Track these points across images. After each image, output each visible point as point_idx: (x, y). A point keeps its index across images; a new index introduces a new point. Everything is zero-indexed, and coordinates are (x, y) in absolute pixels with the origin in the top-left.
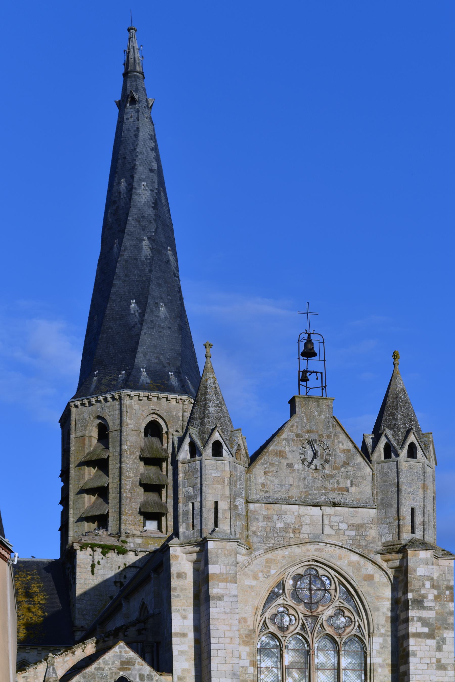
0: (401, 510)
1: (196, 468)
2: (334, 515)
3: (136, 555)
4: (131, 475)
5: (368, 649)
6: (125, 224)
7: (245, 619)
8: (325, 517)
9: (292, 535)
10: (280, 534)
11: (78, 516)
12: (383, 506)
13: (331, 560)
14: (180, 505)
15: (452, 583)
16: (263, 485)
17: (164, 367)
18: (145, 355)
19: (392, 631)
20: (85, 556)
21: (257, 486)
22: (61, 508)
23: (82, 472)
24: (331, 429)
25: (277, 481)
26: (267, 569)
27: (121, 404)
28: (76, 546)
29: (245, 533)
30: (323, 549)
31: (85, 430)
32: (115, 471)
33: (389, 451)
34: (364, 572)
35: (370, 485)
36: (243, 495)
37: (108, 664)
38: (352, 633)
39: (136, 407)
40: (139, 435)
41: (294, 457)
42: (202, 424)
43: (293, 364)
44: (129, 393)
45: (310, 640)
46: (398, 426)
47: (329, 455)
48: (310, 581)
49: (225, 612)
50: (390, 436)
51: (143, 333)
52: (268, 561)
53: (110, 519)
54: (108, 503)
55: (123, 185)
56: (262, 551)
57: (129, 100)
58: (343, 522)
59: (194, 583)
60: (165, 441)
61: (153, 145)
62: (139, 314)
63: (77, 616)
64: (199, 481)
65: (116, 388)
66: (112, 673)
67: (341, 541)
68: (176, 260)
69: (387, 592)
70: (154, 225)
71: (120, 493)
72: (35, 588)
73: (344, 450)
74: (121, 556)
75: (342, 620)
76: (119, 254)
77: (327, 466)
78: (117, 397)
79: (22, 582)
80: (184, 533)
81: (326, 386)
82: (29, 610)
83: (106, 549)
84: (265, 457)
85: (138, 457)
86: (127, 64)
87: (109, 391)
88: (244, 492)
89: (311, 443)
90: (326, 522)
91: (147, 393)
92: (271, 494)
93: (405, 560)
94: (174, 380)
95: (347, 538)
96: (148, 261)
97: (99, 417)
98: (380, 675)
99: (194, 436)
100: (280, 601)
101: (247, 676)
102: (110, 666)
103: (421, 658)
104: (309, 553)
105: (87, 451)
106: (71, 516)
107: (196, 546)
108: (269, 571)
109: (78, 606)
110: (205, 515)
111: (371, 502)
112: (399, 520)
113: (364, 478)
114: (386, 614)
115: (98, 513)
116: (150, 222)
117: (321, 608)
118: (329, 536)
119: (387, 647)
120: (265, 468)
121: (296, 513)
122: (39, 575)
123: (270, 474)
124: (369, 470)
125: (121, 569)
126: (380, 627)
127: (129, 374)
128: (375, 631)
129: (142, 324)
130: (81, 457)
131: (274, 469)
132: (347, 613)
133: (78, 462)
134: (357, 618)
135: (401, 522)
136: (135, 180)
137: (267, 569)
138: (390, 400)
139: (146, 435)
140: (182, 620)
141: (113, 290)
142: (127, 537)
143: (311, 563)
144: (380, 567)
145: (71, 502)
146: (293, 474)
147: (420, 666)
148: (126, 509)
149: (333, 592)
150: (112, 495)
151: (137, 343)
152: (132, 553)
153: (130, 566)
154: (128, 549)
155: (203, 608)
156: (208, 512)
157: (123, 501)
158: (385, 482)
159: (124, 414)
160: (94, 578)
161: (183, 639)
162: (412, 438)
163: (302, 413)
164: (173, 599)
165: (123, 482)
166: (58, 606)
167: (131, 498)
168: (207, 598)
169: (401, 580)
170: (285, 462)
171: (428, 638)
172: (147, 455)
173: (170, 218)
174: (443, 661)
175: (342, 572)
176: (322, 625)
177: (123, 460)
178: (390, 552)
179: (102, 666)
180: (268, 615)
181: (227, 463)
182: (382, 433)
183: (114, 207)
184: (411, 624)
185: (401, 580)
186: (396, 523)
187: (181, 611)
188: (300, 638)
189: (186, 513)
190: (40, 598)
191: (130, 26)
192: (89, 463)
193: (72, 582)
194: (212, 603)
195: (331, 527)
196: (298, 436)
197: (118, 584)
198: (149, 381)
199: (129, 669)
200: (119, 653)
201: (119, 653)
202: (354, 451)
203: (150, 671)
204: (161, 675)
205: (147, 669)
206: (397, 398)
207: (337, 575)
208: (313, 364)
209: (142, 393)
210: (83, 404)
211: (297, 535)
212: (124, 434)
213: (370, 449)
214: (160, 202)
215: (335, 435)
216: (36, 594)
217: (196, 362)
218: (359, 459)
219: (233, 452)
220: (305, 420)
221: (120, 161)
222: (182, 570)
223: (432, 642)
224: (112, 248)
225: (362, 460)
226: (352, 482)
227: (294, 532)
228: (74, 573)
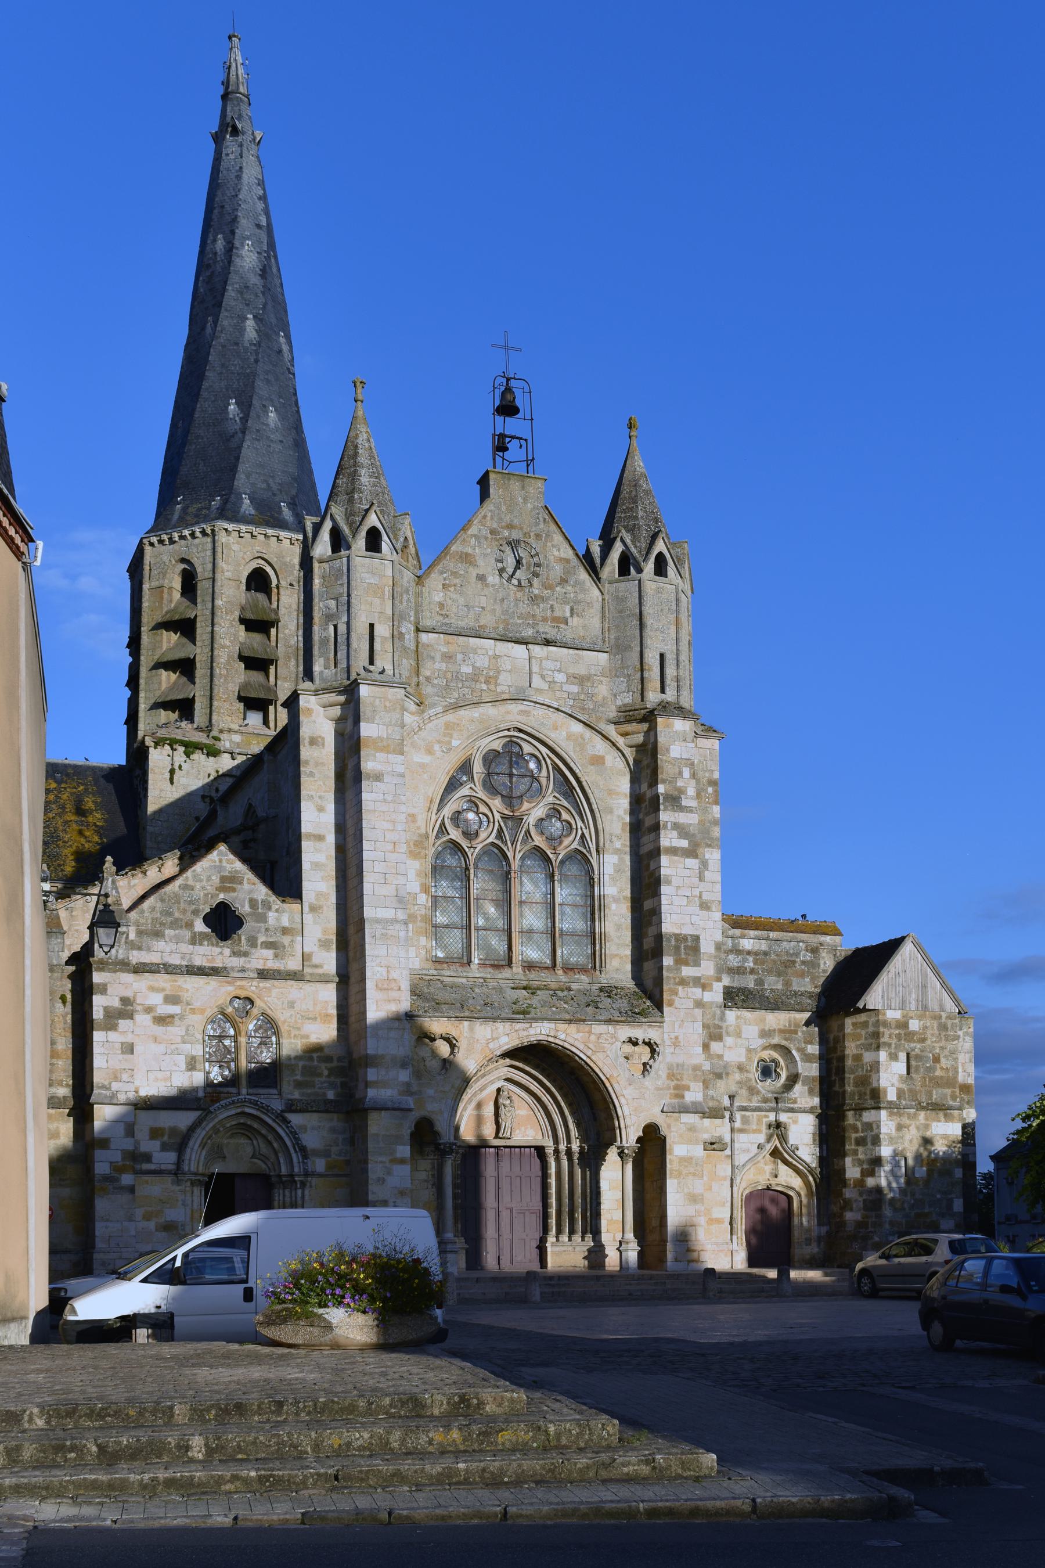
0: (646, 655)
1: (340, 570)
2: (547, 658)
3: (233, 759)
4: (228, 643)
5: (596, 872)
6: (223, 295)
7: (412, 817)
8: (533, 661)
9: (484, 687)
10: (467, 684)
11: (152, 701)
12: (618, 649)
13: (542, 730)
14: (316, 629)
15: (716, 775)
16: (441, 605)
17: (274, 495)
18: (248, 476)
19: (631, 847)
20: (161, 757)
21: (432, 606)
22: (128, 693)
23: (158, 638)
24: (542, 526)
25: (461, 601)
26: (447, 739)
27: (214, 542)
28: (149, 742)
29: (415, 680)
30: (529, 712)
31: (163, 579)
32: (204, 637)
33: (626, 564)
34: (590, 751)
35: (599, 615)
36: (412, 619)
37: (201, 881)
38: (572, 847)
39: (235, 547)
40: (239, 587)
41: (486, 565)
42: (351, 500)
43: (487, 424)
44: (226, 525)
45: (510, 855)
46: (639, 528)
47: (538, 565)
48: (511, 761)
49: (385, 801)
50: (628, 541)
51: (245, 445)
52: (448, 726)
53: (198, 706)
54: (194, 683)
55: (220, 244)
56: (439, 709)
57: (230, 129)
58: (560, 671)
59: (336, 754)
60: (274, 598)
61: (261, 192)
62: (241, 419)
63: (149, 844)
64: (346, 590)
65: (207, 519)
66: (206, 895)
67: (557, 700)
68: (291, 351)
69: (624, 785)
70: (262, 299)
71: (212, 668)
72: (89, 803)
73: (561, 559)
74: (211, 758)
75: (556, 827)
76: (213, 336)
77: (536, 582)
78: (209, 531)
79: (72, 794)
80: (321, 673)
81: (533, 459)
82: (81, 833)
83: (190, 748)
84: (445, 562)
85: (237, 619)
86: (226, 84)
87: (197, 523)
88: (412, 613)
89: (513, 544)
90: (535, 669)
91: (251, 528)
92: (453, 621)
93: (652, 733)
94: (287, 514)
95: (565, 695)
96: (254, 348)
97: (183, 560)
99: (338, 518)
100: (465, 791)
101: (416, 908)
102: (204, 883)
103: (678, 888)
104: (510, 717)
105: (165, 609)
106: (141, 700)
107: (340, 693)
108: (450, 743)
109: (150, 829)
110: (354, 644)
111: (600, 642)
112: (642, 670)
113: (589, 604)
114: (623, 819)
115: (180, 697)
116: (256, 296)
117: (526, 806)
118: (539, 691)
119: (624, 871)
120: (445, 579)
121: (491, 653)
122: (95, 785)
123: (452, 589)
124: (597, 592)
125: (212, 778)
126: (614, 839)
127: (225, 502)
128: (607, 845)
129: (244, 433)
130: (159, 618)
131: (457, 581)
132: (565, 816)
133: (154, 624)
134: (580, 824)
135: (646, 674)
136: (237, 236)
137: (447, 739)
138: (625, 489)
139: (248, 589)
140: (316, 813)
141: (206, 384)
142: (221, 731)
143: (512, 733)
144: (614, 744)
145: (142, 681)
146: (486, 592)
147: (676, 900)
148: (219, 691)
149: (544, 781)
150: (201, 672)
151: (237, 458)
152: (227, 756)
153: (224, 775)
154: (222, 749)
155: (349, 795)
156: (359, 639)
157: (215, 680)
158: (620, 612)
159: (219, 555)
160: (174, 789)
161: (318, 844)
162: (660, 546)
163: (499, 497)
164: (304, 779)
165: (216, 653)
166: (122, 829)
167: (226, 677)
168: (358, 777)
169: (646, 765)
170: (474, 572)
171: (688, 857)
172: (249, 616)
173: (283, 294)
174: (705, 897)
175: (558, 750)
176: (528, 832)
177: (216, 620)
178: (629, 720)
179: (190, 882)
180: (448, 811)
181: (389, 564)
182: (615, 539)
183: (208, 273)
184: (662, 832)
185: (646, 765)
186: (639, 674)
187: (317, 799)
188: (496, 851)
189: (324, 641)
190: (97, 818)
191: (231, 33)
192: (168, 625)
193: (142, 796)
194: (365, 784)
195: (543, 677)
196: (493, 532)
197: (207, 800)
198: (253, 512)
199: (234, 890)
200: (217, 863)
201: (217, 863)
202: (575, 561)
203: (267, 894)
204: (284, 901)
205: (262, 891)
206: (635, 485)
207: (551, 755)
208: (512, 425)
209: (243, 528)
210: (161, 542)
211: (492, 687)
212: (218, 584)
213: (598, 561)
214: (267, 270)
215: (547, 536)
216: (91, 812)
217: (316, 495)
218: (583, 575)
219: (399, 546)
220: (504, 508)
221: (216, 211)
222: (318, 733)
223: (692, 863)
224: (203, 328)
225: (587, 576)
226: (572, 610)
227: (487, 682)
228: (145, 782)
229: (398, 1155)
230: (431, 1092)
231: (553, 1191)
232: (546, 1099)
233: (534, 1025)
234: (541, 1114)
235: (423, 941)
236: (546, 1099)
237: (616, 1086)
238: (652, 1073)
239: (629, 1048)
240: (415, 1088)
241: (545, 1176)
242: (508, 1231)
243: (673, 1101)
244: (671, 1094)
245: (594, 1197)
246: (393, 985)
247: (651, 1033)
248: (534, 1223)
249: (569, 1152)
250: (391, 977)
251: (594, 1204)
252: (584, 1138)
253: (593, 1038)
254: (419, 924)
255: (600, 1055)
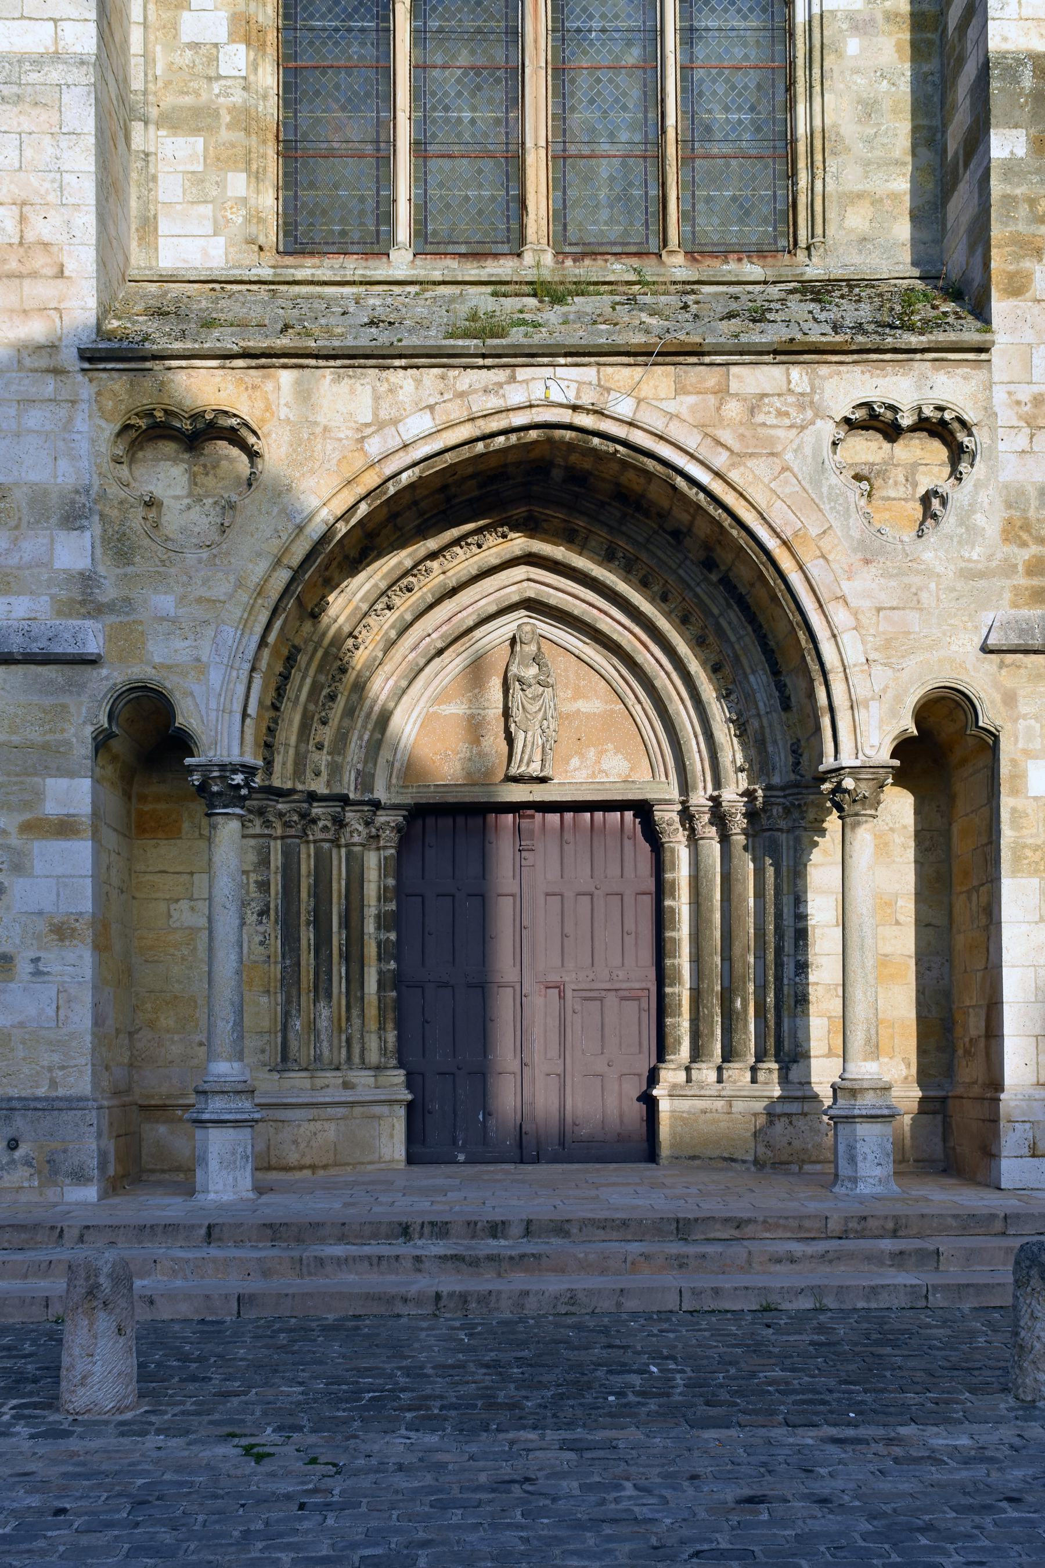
98: (857, 71)
101: (216, 88)
229: (52, 808)
230: (165, 602)
231: (682, 932)
232: (650, 657)
233: (522, 373)
234: (643, 709)
235: (238, 183)
236: (650, 657)
237: (815, 569)
238: (949, 520)
239: (868, 448)
240: (108, 592)
241: (661, 889)
242: (554, 1052)
243: (1025, 612)
244: (1016, 590)
245: (788, 946)
246: (40, 261)
247: (948, 388)
248: (633, 1022)
249: (719, 817)
250: (30, 236)
251: (789, 969)
252: (758, 765)
253: (733, 409)
254: (225, 135)
255: (761, 467)
